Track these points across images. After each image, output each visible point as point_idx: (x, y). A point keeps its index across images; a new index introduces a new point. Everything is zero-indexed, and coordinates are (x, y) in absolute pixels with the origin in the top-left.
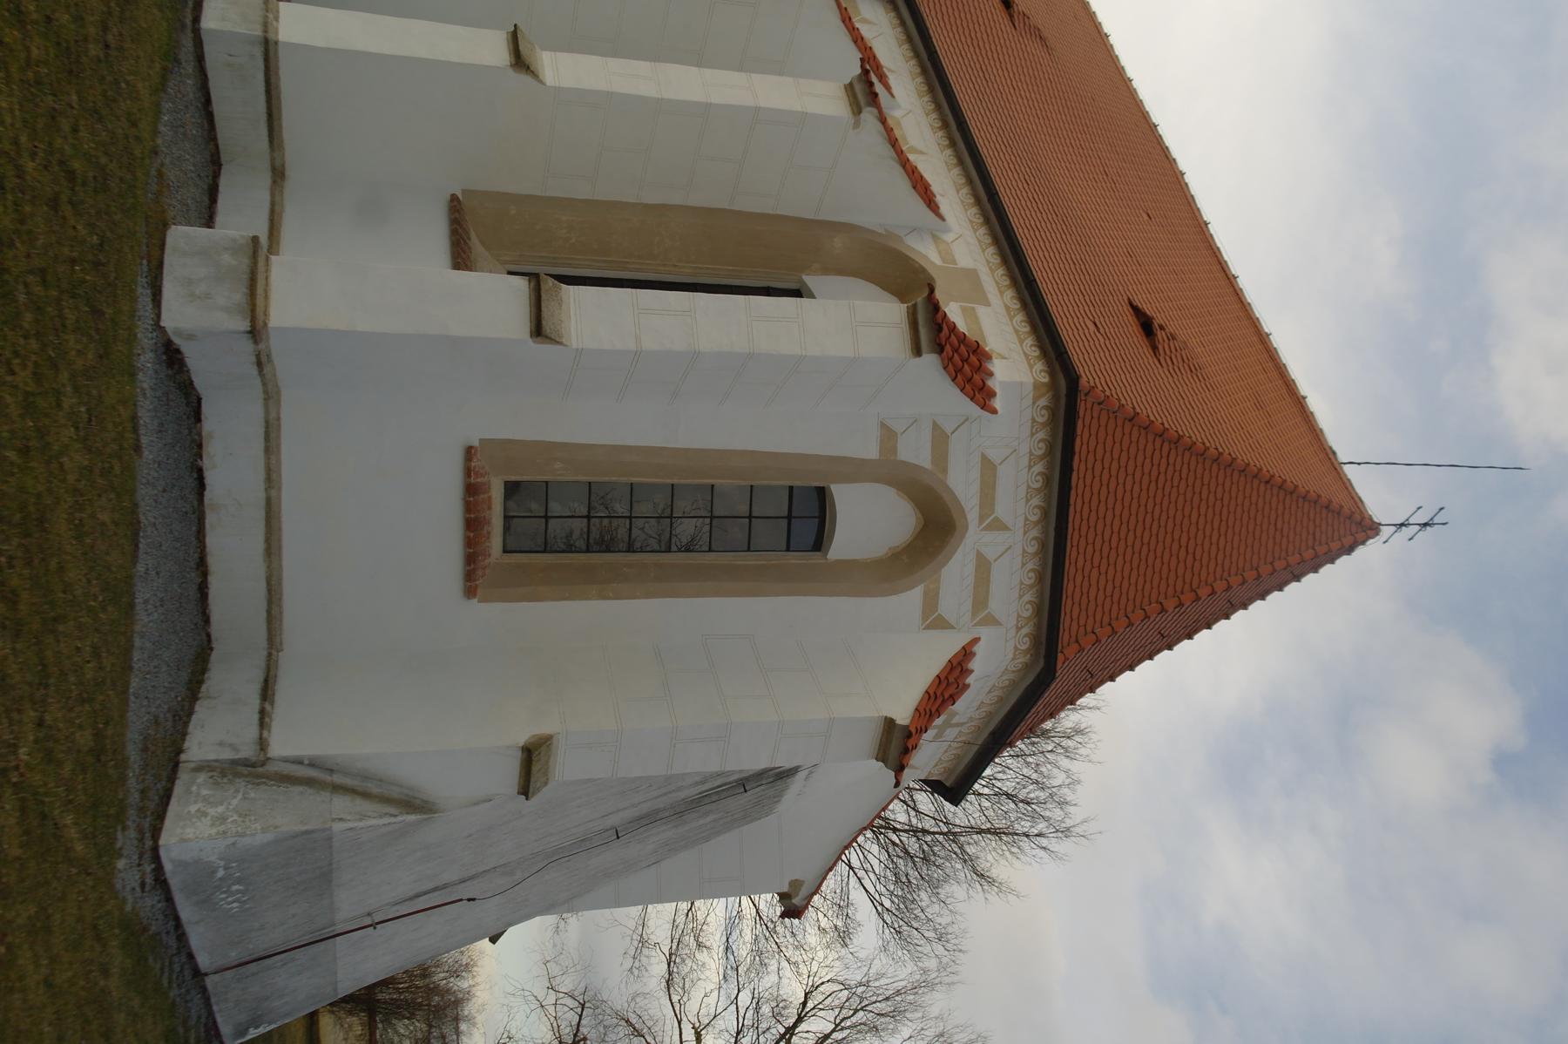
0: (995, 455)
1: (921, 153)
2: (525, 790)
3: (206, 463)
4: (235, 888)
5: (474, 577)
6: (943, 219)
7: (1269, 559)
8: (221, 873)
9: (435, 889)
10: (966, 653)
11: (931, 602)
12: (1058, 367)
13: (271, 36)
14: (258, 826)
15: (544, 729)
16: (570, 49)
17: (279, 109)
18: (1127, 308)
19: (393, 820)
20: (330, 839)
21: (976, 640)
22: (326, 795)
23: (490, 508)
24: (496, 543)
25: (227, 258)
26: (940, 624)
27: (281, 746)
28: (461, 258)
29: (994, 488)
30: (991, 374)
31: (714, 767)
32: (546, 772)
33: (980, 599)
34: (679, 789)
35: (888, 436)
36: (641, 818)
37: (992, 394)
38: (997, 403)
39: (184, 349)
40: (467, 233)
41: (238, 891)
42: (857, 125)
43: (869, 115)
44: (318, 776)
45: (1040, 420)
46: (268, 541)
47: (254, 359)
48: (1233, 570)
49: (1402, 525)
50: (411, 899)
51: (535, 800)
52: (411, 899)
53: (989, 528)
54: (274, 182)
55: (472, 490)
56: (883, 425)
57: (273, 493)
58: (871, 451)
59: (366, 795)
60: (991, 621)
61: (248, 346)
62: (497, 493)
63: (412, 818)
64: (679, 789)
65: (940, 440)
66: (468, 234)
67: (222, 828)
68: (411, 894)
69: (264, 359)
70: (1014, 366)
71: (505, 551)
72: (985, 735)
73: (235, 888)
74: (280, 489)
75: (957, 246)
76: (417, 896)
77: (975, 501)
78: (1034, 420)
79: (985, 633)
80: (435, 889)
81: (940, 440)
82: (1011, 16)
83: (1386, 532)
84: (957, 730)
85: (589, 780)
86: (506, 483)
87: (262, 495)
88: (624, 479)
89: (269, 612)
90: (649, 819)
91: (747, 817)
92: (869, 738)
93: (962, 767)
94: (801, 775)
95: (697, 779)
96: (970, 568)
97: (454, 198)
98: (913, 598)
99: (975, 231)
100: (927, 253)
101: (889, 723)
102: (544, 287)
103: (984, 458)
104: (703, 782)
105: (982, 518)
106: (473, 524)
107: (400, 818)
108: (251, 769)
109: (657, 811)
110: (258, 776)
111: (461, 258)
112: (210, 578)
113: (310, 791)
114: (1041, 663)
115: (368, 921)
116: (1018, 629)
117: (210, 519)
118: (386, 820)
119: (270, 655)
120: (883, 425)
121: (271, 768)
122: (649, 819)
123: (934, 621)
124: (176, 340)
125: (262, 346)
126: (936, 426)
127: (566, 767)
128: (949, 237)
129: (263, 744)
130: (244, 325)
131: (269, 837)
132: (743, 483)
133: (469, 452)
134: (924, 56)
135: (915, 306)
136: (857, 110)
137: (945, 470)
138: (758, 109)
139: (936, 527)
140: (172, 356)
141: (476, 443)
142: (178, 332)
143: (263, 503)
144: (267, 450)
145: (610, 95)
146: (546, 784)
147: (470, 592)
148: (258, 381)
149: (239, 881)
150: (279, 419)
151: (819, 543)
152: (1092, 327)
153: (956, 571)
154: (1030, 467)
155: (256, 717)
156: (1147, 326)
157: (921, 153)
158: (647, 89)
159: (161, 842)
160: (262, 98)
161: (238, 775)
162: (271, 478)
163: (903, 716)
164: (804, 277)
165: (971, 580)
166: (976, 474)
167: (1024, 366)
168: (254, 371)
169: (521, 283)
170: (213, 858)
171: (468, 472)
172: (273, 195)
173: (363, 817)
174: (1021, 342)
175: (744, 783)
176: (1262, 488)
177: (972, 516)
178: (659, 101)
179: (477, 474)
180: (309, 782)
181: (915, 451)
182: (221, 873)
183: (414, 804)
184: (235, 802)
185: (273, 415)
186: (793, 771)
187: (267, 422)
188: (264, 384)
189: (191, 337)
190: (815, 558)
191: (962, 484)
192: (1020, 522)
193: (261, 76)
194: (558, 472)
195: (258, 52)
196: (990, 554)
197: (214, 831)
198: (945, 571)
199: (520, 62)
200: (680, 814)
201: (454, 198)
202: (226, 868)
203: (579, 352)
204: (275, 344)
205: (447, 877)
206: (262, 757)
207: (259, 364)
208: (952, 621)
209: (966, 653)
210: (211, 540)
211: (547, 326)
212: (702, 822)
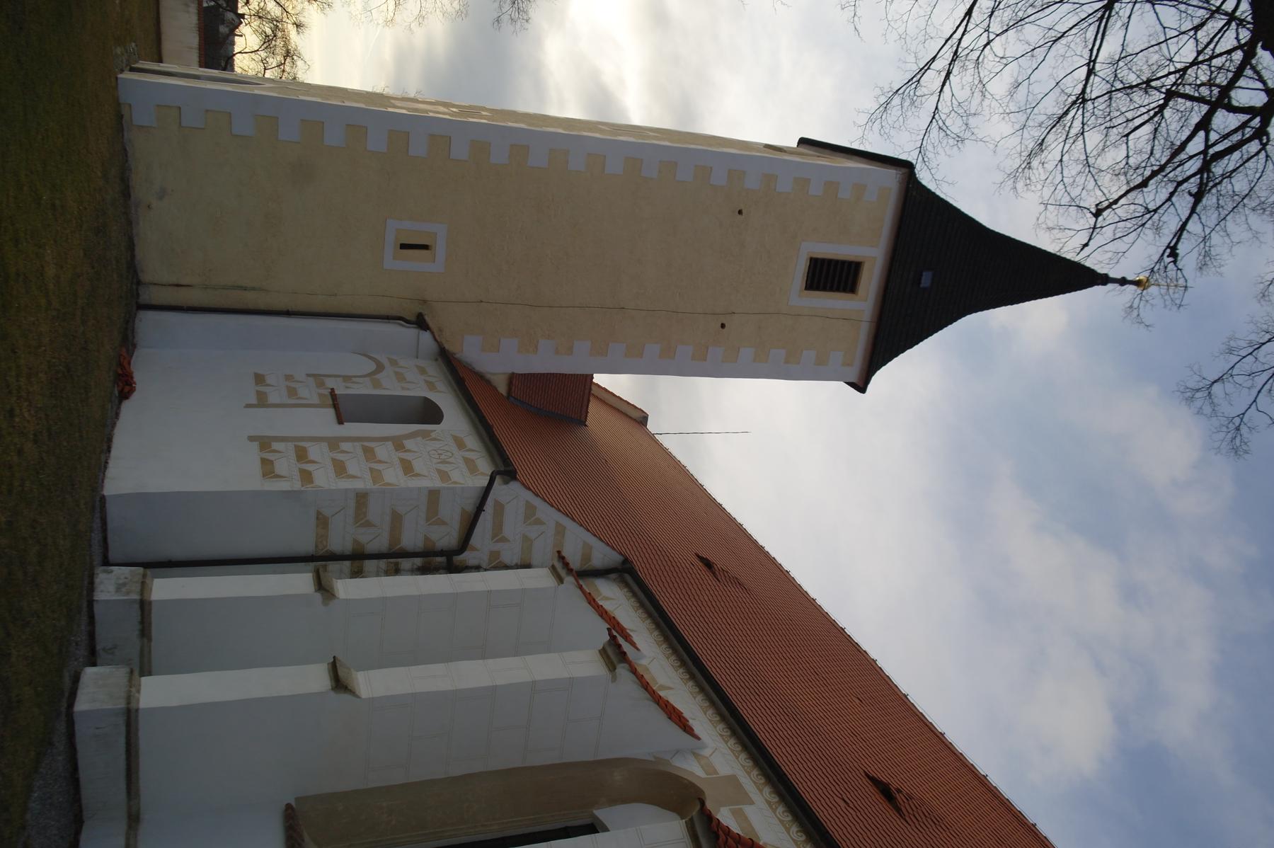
1: (670, 688)
13: (133, 705)
42: (614, 679)
43: (622, 670)
82: (714, 574)
97: (289, 807)
100: (692, 769)
128: (706, 752)
135: (691, 819)
138: (534, 682)
157: (670, 688)
158: (444, 685)
160: (123, 757)
199: (340, 684)
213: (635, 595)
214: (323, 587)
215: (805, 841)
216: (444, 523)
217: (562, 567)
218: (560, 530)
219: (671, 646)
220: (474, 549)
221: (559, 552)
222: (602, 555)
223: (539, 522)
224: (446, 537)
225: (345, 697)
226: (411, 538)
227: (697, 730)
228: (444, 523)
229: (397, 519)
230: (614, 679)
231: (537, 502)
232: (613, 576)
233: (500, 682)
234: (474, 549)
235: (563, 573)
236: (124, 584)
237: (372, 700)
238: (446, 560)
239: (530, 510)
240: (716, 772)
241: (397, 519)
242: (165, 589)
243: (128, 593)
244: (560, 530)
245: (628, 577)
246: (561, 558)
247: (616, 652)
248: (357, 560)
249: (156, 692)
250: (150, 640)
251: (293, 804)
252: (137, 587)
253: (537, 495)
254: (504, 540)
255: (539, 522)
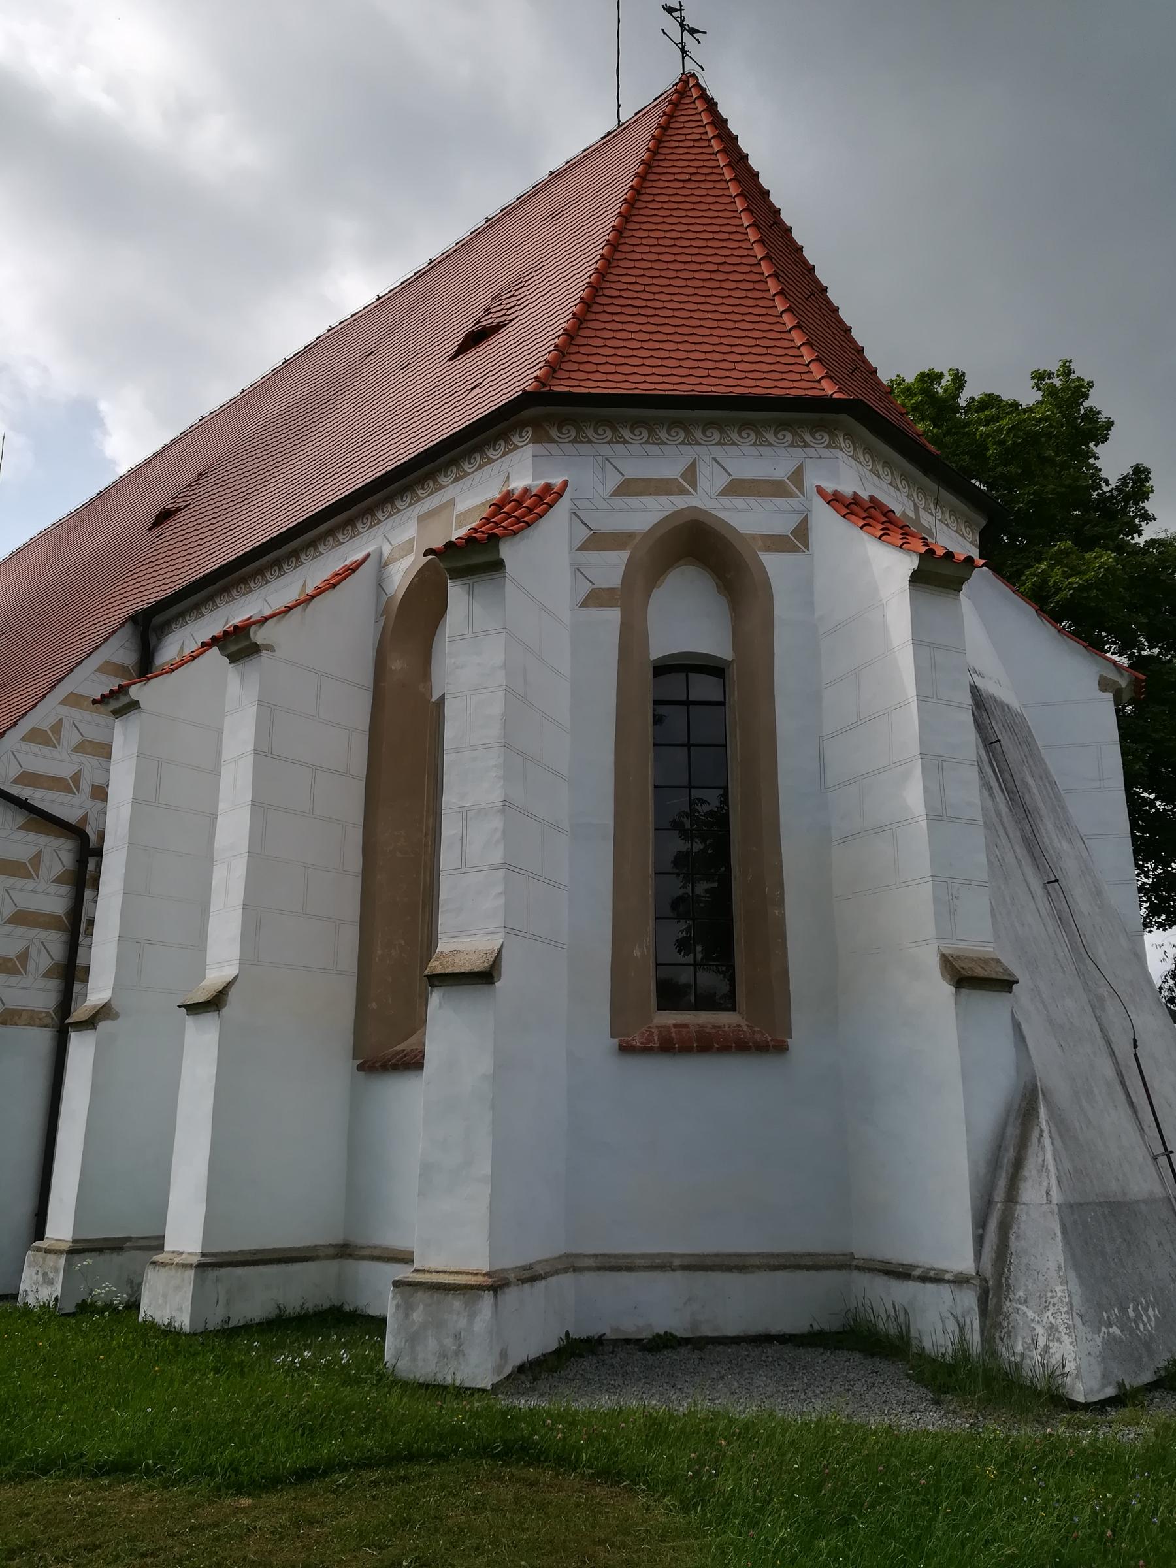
0: (613, 481)
1: (305, 584)
2: (1006, 984)
3: (646, 1335)
4: (1131, 1314)
5: (767, 1043)
6: (368, 555)
7: (723, 185)
8: (1115, 1330)
9: (1123, 1084)
10: (835, 500)
11: (778, 544)
12: (513, 419)
13: (195, 1260)
14: (1059, 1288)
15: (934, 963)
16: (204, 949)
17: (275, 1250)
18: (462, 359)
19: (1046, 1134)
20: (1071, 1206)
21: (820, 490)
22: (1020, 1210)
23: (686, 1026)
24: (725, 1019)
25: (417, 1316)
26: (802, 533)
27: (963, 1261)
28: (413, 1063)
29: (648, 481)
30: (526, 490)
31: (972, 774)
32: (985, 962)
33: (775, 489)
34: (999, 814)
35: (596, 598)
36: (1034, 858)
37: (548, 488)
38: (557, 481)
39: (518, 1363)
40: (398, 1053)
41: (1135, 1309)
42: (270, 648)
43: (259, 636)
44: (996, 1211)
45: (573, 434)
46: (729, 1269)
47: (527, 1286)
48: (737, 222)
49: (683, 51)
50: (1135, 1112)
51: (1018, 972)
52: (1135, 1112)
53: (694, 485)
54: (350, 1256)
55: (669, 1046)
56: (584, 604)
57: (677, 1262)
58: (613, 615)
59: (1018, 1164)
60: (797, 476)
61: (511, 1295)
62: (670, 1018)
63: (1043, 1113)
64: (999, 814)
65: (597, 542)
66: (386, 1050)
67: (1062, 1328)
68: (1129, 1111)
69: (527, 1274)
70: (519, 469)
71: (735, 1010)
72: (926, 481)
73: (1131, 1314)
74: (673, 1256)
75: (399, 545)
76: (1131, 1104)
77: (664, 500)
78: (574, 441)
79: (814, 479)
80: (1123, 1084)
81: (597, 542)
82: (178, 510)
83: (690, 67)
84: (923, 513)
85: (993, 915)
86: (660, 1008)
87: (679, 1274)
88: (651, 882)
89: (808, 1268)
90: (1033, 846)
91: (1027, 741)
92: (938, 603)
93: (963, 507)
94: (979, 682)
95: (986, 793)
96: (739, 502)
97: (360, 1068)
98: (773, 563)
99: (380, 521)
100: (402, 573)
101: (917, 579)
102: (439, 970)
103: (617, 493)
104: (989, 788)
105: (683, 492)
106: (705, 1045)
107: (1044, 1126)
108: (992, 1291)
109: (1025, 839)
110: (999, 1285)
111: (413, 1063)
112: (773, 1332)
113: (1015, 1228)
114: (844, 417)
115: (1163, 1160)
116: (806, 445)
117: (707, 1331)
118: (1047, 1141)
119: (858, 1268)
120: (584, 604)
121: (988, 1268)
122: (1033, 846)
123: (799, 538)
124: (508, 1370)
125: (512, 1277)
126: (583, 548)
127: (978, 939)
128: (387, 550)
129: (960, 1281)
130: (488, 1297)
131: (1072, 1275)
132: (651, 755)
133: (626, 1049)
134: (211, 589)
135: (450, 571)
136: (255, 650)
137: (631, 535)
138: (256, 752)
139: (699, 546)
140: (533, 1372)
141: (616, 1041)
142: (498, 1369)
143: (687, 1274)
144: (629, 1269)
145: (246, 907)
146: (998, 961)
147: (781, 1048)
148: (553, 1280)
149: (1123, 1310)
150: (596, 1256)
151: (714, 668)
152: (477, 390)
153: (746, 518)
154: (625, 442)
155: (930, 1286)
156: (475, 339)
157: (305, 584)
158: (240, 868)
159: (1082, 1400)
160: (262, 1269)
161: (999, 1310)
162: (660, 1264)
163: (907, 564)
164: (433, 700)
165: (752, 501)
166: (633, 501)
167: (516, 456)
168: (541, 1284)
169: (435, 999)
170: (1099, 1340)
171: (645, 1050)
172: (363, 1258)
173: (1043, 1166)
174: (492, 461)
175: (989, 743)
176: (643, 198)
177: (681, 502)
178: (251, 854)
179: (648, 1041)
180: (1005, 1229)
181: (610, 568)
182: (1115, 1330)
183: (1026, 1107)
184: (1030, 1314)
185: (591, 1262)
186: (974, 690)
187: (599, 1269)
188: (557, 1272)
189: (504, 1355)
190: (733, 673)
191: (646, 515)
192: (686, 449)
193: (239, 1271)
194: (642, 951)
195: (212, 1274)
196: (722, 481)
197: (1067, 1340)
198: (742, 529)
199: (215, 1003)
200: (1027, 812)
201: (360, 1068)
202: (1110, 1325)
203: (509, 931)
204: (510, 1261)
205: (1109, 1071)
206: (976, 1282)
207: (533, 1279)
208: (798, 519)
209: (835, 500)
210: (731, 1331)
211: (480, 965)
212: (1035, 791)
213: (182, 615)
214: (90, 1023)
215: (1025, 1179)
216: (38, 855)
217: (115, 702)
218: (73, 700)
219: (253, 576)
220: (84, 818)
221: (95, 702)
222: (121, 651)
223: (57, 727)
224: (58, 854)
225: (233, 995)
226: (52, 900)
227: (359, 556)
228: (38, 855)
229: (22, 918)
230: (270, 648)
231: (25, 726)
232: (153, 640)
233: (249, 798)
234: (84, 818)
235: (123, 700)
236: (45, 1274)
237: (242, 962)
238: (87, 852)
239: (35, 736)
240: (411, 540)
241: (22, 918)
242: (61, 1227)
243: (56, 1270)
244: (73, 700)
245: (158, 620)
246: (104, 700)
247: (238, 644)
248: (71, 972)
249: (185, 1236)
250: (129, 1239)
251: (359, 1062)
252: (51, 1258)
253: (15, 724)
254: (77, 778)
255: (57, 727)
